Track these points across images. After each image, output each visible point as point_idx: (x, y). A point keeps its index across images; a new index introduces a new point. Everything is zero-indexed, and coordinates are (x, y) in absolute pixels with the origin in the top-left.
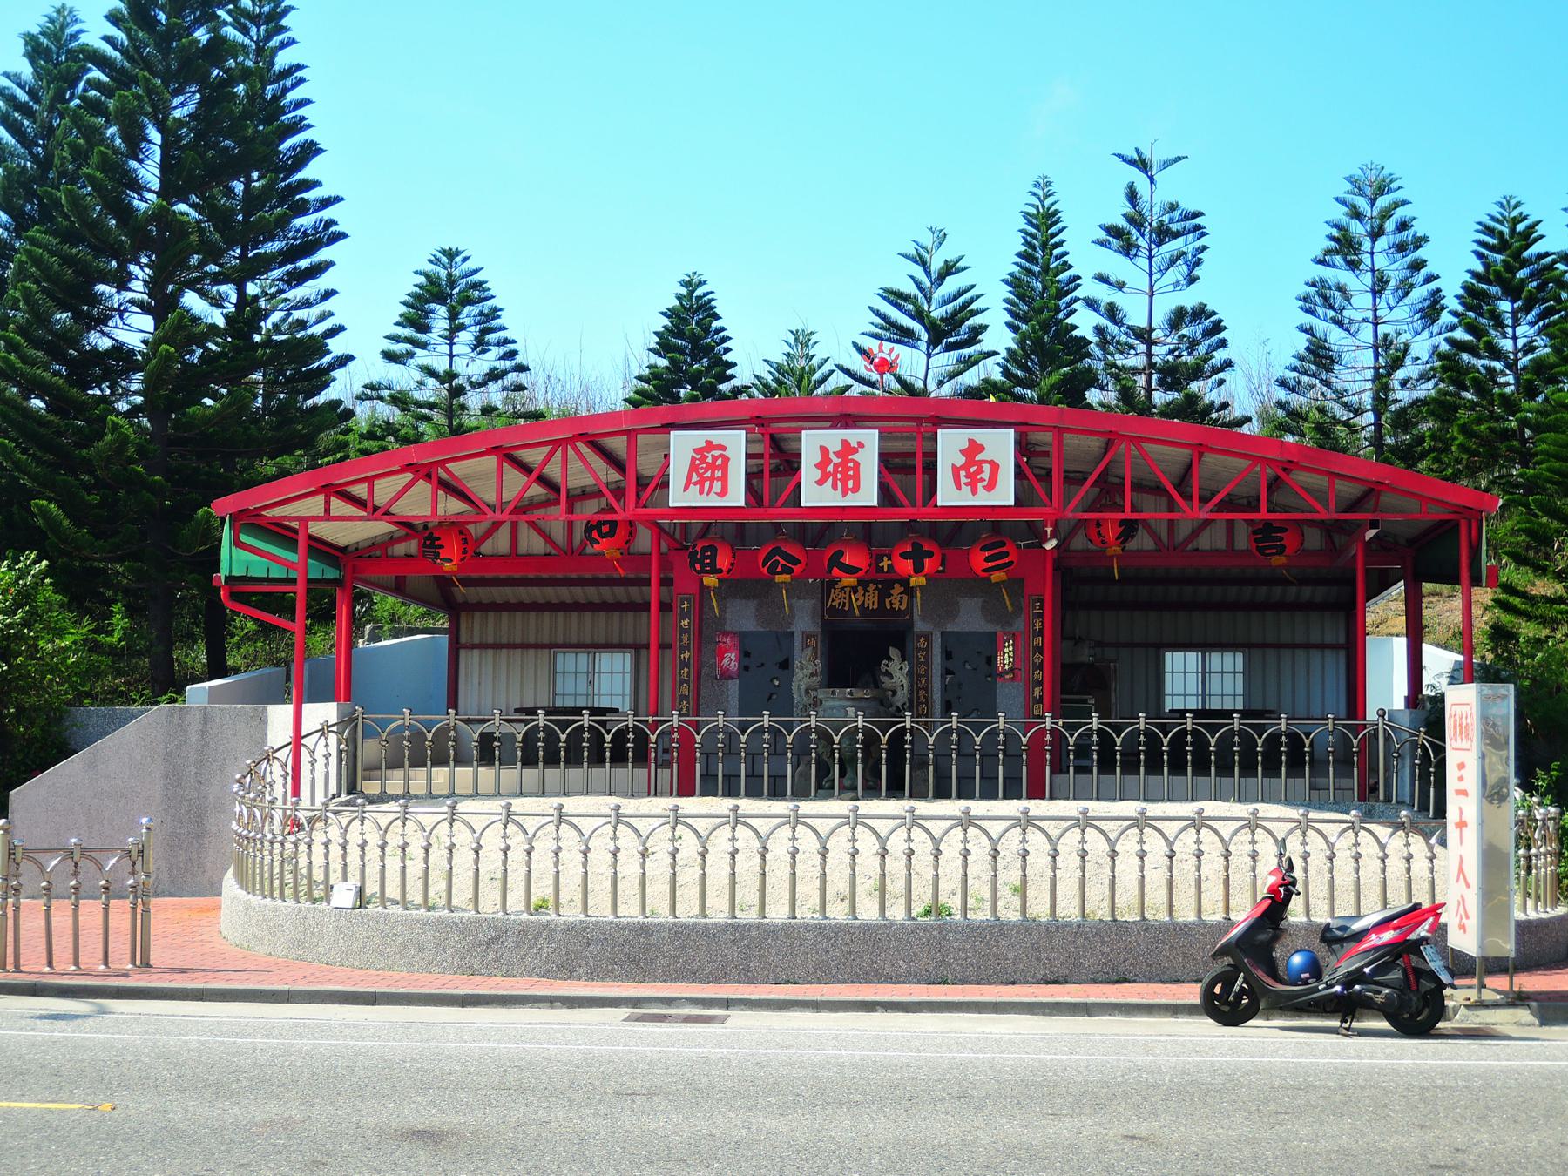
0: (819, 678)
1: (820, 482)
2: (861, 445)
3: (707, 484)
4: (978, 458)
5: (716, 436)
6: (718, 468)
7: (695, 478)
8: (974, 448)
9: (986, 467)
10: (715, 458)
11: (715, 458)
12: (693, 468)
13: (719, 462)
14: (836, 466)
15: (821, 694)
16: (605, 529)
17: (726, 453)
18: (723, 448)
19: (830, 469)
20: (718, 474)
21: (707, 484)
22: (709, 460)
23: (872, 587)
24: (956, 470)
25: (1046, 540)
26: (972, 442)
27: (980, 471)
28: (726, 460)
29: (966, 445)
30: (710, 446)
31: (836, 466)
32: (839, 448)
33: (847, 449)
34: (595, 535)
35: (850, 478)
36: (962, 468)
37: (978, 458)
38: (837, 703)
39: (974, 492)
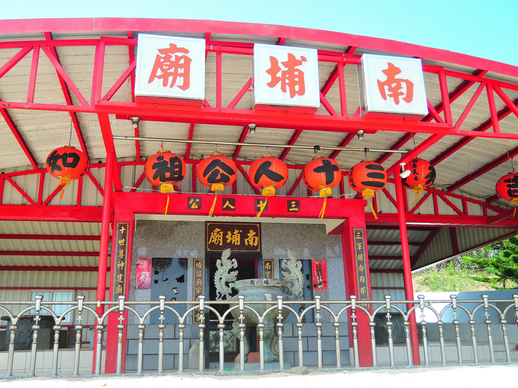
0: (236, 273)
1: (271, 85)
2: (304, 59)
3: (171, 79)
4: (397, 77)
5: (180, 42)
6: (181, 66)
7: (159, 72)
8: (392, 71)
9: (404, 85)
10: (178, 58)
11: (178, 58)
12: (158, 64)
13: (182, 61)
14: (284, 73)
15: (239, 285)
16: (70, 160)
17: (188, 55)
18: (187, 51)
19: (279, 75)
20: (181, 71)
21: (171, 79)
22: (173, 59)
23: (236, 232)
24: (381, 85)
25: (401, 172)
26: (390, 65)
27: (399, 87)
28: (188, 61)
29: (386, 67)
30: (173, 48)
31: (284, 73)
32: (286, 59)
33: (292, 62)
34: (60, 162)
35: (297, 83)
36: (385, 83)
37: (397, 77)
38: (255, 291)
39: (397, 102)
